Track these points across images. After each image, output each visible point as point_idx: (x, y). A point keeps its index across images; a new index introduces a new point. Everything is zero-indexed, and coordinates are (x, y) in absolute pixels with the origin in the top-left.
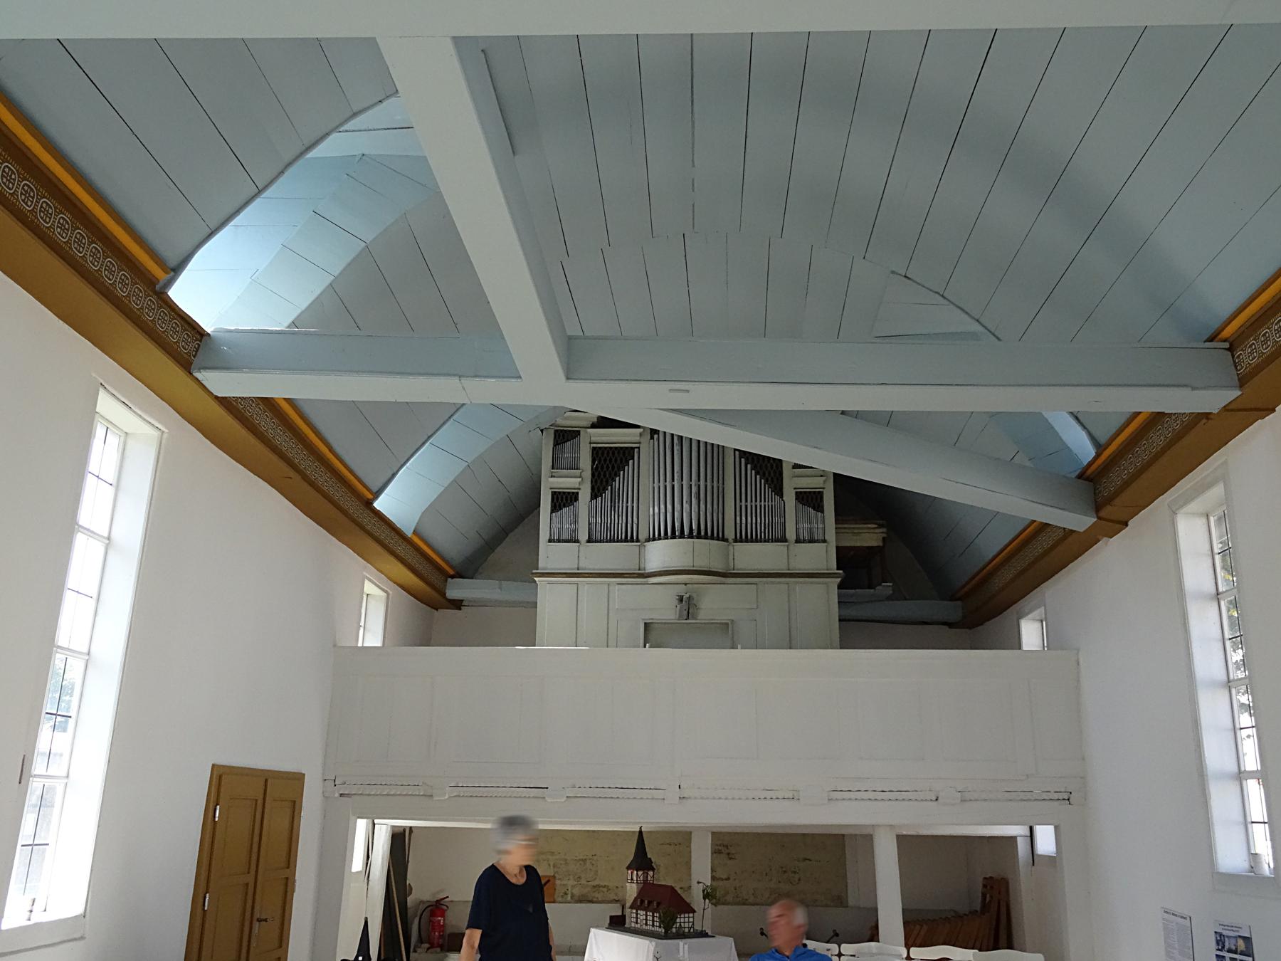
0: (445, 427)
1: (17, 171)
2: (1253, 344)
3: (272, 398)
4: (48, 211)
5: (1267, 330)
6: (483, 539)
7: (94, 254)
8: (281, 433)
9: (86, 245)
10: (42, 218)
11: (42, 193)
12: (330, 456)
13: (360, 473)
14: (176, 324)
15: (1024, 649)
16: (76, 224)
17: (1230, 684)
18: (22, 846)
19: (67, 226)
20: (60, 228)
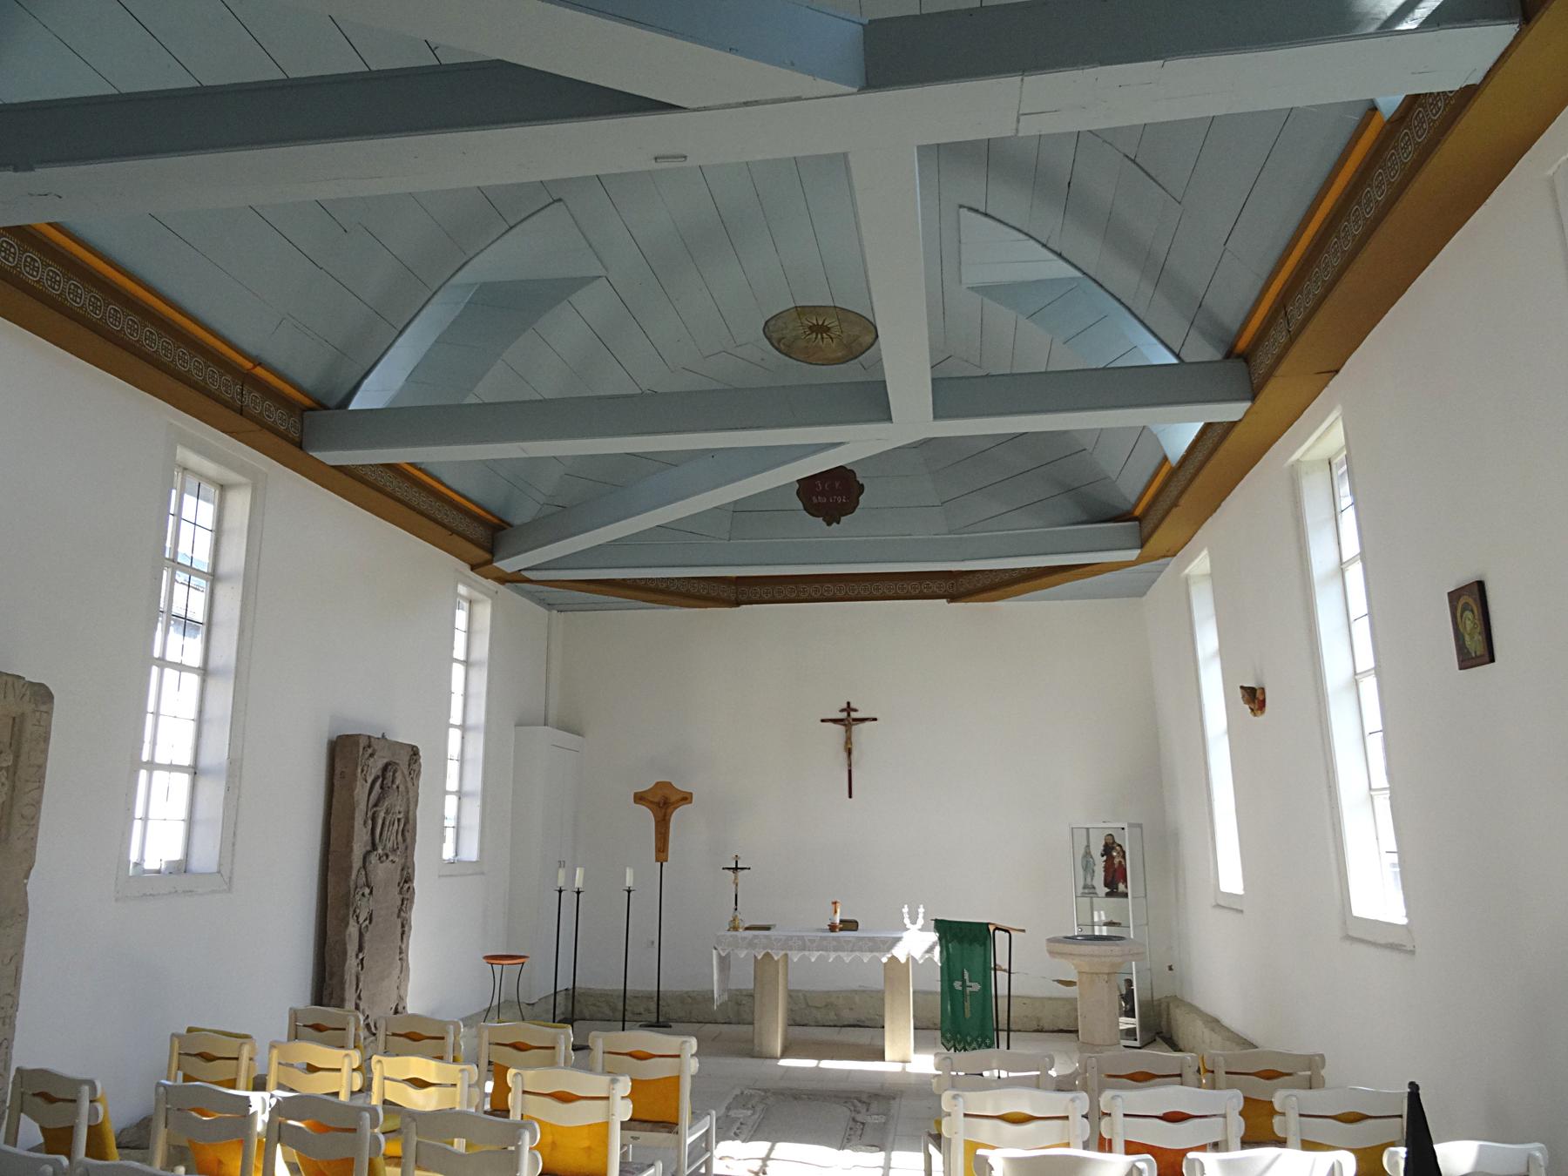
0: (429, 308)
1: (82, 285)
2: (1420, 111)
3: (29, 226)
4: (77, 292)
5: (1420, 109)
6: (1152, 997)
7: (52, 278)
8: (379, 479)
9: (67, 291)
10: (28, 273)
11: (23, 247)
12: (442, 489)
13: (190, 304)
14: (95, 297)
15: (751, 986)
16: (23, 247)
17: (1357, 677)
18: (339, 1070)
19: (12, 250)
20: (130, 329)
